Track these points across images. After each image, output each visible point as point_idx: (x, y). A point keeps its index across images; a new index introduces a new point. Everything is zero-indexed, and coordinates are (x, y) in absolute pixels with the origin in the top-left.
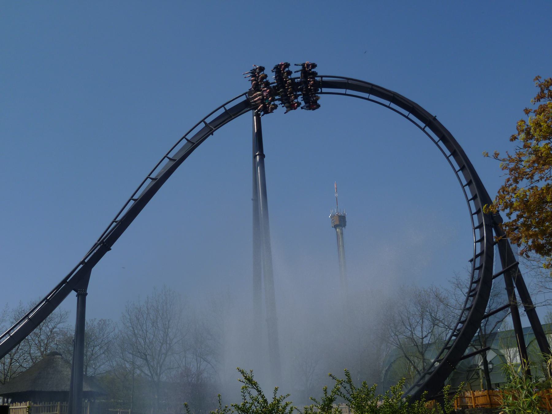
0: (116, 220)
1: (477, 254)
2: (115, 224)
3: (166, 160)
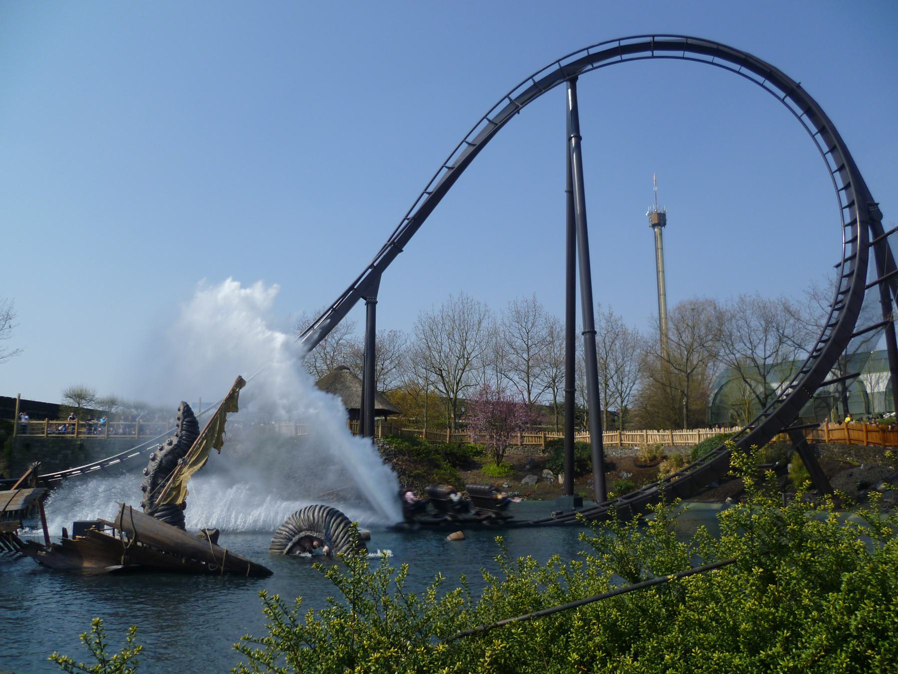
0: (408, 217)
1: (846, 257)
2: (406, 222)
3: (465, 145)
